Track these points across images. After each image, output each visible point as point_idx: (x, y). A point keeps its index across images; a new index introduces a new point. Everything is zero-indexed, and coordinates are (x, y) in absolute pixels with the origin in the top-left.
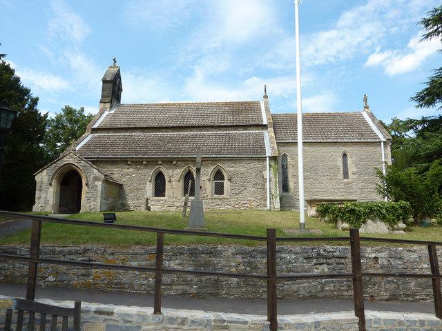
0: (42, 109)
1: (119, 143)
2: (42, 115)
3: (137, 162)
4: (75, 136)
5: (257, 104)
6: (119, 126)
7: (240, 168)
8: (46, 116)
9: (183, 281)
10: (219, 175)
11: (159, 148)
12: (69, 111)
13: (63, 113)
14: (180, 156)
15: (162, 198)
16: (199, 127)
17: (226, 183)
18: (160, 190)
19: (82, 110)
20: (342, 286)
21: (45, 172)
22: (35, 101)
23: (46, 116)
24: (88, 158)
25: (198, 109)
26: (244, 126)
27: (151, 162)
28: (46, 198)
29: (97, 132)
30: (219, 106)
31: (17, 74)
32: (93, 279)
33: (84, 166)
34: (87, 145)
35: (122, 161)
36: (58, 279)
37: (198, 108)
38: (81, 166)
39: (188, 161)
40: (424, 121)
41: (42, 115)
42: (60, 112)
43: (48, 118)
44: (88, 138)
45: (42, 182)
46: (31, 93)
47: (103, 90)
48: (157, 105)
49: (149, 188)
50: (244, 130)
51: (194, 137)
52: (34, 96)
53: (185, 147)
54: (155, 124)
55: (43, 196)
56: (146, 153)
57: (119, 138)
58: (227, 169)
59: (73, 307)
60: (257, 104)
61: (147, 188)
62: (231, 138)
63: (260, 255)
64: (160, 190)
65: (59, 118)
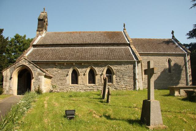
0: (5, 35)
1: (50, 54)
2: (5, 38)
3: (61, 64)
4: (23, 50)
7: (122, 68)
8: (7, 38)
10: (109, 72)
11: (73, 55)
12: (17, 37)
13: (14, 38)
14: (86, 60)
15: (88, 82)
16: (93, 44)
18: (75, 80)
19: (25, 36)
21: (8, 70)
23: (7, 38)
24: (34, 62)
25: (90, 35)
26: (117, 44)
27: (68, 65)
29: (36, 47)
30: (101, 34)
34: (31, 54)
35: (52, 63)
37: (90, 34)
38: (30, 66)
40: (191, 44)
41: (5, 38)
42: (13, 37)
43: (27, 38)
44: (31, 49)
45: (7, 76)
47: (39, 24)
48: (68, 33)
49: (69, 79)
50: (117, 46)
53: (88, 55)
54: (68, 42)
55: (8, 84)
56: (66, 59)
58: (114, 68)
59: (169, 90)
62: (112, 51)
64: (75, 80)
65: (12, 40)
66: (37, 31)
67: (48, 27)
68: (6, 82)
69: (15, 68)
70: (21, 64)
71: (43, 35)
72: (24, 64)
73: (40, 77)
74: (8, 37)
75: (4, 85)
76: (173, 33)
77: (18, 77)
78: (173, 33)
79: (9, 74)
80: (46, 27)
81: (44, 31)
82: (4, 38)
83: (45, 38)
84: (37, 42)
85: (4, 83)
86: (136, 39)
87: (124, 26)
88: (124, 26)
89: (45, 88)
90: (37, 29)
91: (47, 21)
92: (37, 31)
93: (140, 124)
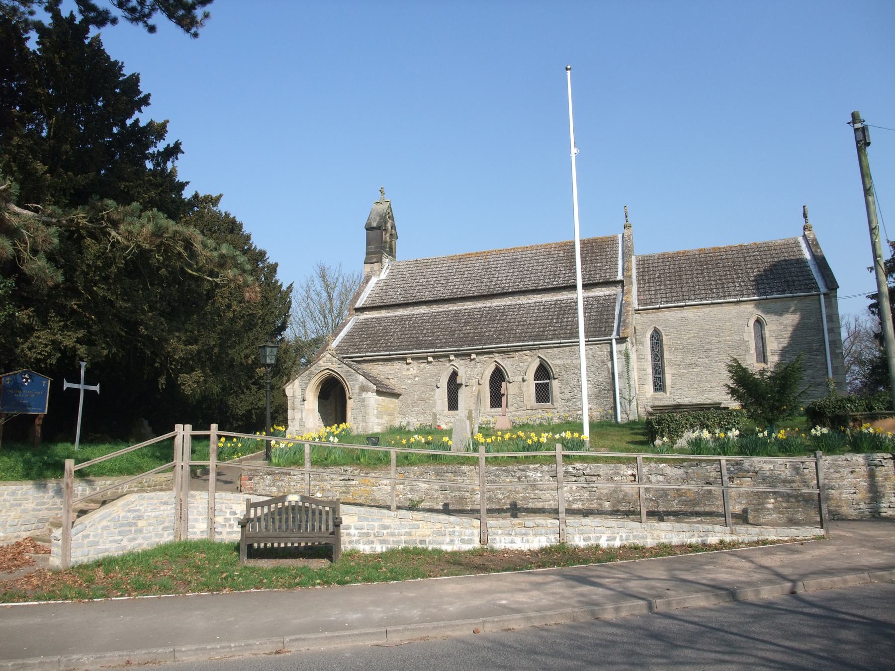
2: (284, 288)
5: (613, 241)
6: (394, 301)
9: (430, 498)
15: (489, 404)
17: (555, 384)
20: (591, 504)
21: (297, 382)
22: (273, 268)
28: (301, 420)
31: (246, 230)
32: (352, 495)
33: (347, 372)
36: (324, 495)
39: (492, 353)
41: (284, 288)
46: (267, 256)
47: (368, 243)
51: (507, 309)
52: (271, 261)
55: (298, 416)
57: (394, 320)
60: (613, 241)
61: (436, 397)
63: (504, 474)
66: (365, 263)
67: (400, 246)
68: (294, 409)
69: (310, 378)
70: (323, 368)
71: (383, 276)
72: (330, 366)
73: (364, 395)
74: (291, 285)
75: (289, 417)
76: (804, 207)
77: (319, 398)
78: (804, 207)
79: (298, 394)
80: (391, 248)
81: (386, 261)
82: (281, 285)
83: (387, 285)
84: (365, 299)
85: (290, 412)
86: (663, 255)
87: (805, 216)
88: (805, 216)
89: (380, 421)
90: (364, 256)
91: (393, 227)
92: (365, 263)
93: (97, 26)
